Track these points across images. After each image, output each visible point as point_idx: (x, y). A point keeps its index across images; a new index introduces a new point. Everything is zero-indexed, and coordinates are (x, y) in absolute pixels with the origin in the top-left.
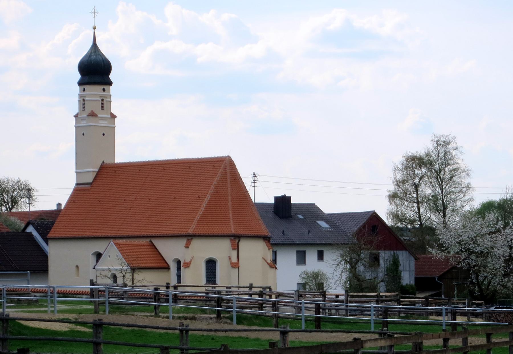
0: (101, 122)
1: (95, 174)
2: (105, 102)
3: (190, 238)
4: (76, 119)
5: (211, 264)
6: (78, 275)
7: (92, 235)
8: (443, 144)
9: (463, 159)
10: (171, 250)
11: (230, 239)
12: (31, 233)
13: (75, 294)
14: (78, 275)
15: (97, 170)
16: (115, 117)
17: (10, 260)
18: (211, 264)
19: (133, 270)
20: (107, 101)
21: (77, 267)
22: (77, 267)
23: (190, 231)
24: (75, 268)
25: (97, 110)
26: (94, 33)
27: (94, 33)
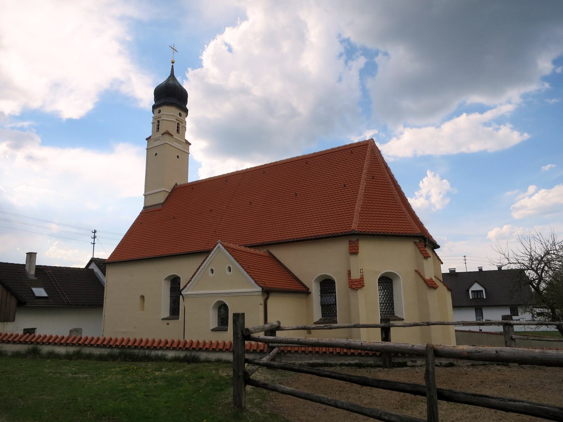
0: (175, 143)
1: (168, 194)
2: (180, 126)
3: (354, 239)
4: (148, 142)
5: (387, 281)
6: (143, 308)
7: (167, 253)
8: (81, 329)
9: (70, 329)
10: (309, 263)
11: (415, 243)
12: (93, 270)
13: (148, 348)
14: (143, 308)
15: (170, 191)
16: (190, 144)
17: (62, 294)
18: (387, 281)
19: (267, 292)
20: (183, 126)
21: (142, 297)
22: (142, 297)
23: (355, 227)
24: (138, 300)
25: (173, 131)
26: (173, 66)
27: (173, 66)
